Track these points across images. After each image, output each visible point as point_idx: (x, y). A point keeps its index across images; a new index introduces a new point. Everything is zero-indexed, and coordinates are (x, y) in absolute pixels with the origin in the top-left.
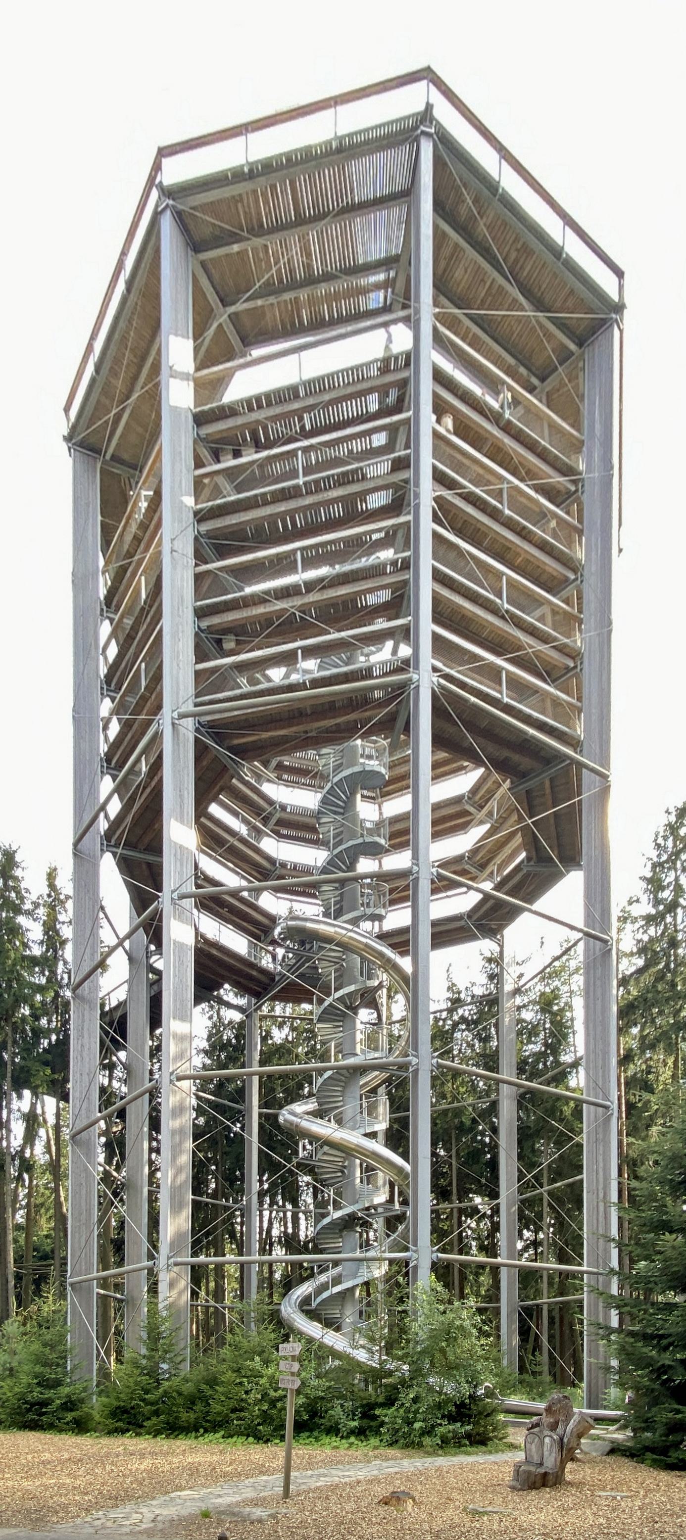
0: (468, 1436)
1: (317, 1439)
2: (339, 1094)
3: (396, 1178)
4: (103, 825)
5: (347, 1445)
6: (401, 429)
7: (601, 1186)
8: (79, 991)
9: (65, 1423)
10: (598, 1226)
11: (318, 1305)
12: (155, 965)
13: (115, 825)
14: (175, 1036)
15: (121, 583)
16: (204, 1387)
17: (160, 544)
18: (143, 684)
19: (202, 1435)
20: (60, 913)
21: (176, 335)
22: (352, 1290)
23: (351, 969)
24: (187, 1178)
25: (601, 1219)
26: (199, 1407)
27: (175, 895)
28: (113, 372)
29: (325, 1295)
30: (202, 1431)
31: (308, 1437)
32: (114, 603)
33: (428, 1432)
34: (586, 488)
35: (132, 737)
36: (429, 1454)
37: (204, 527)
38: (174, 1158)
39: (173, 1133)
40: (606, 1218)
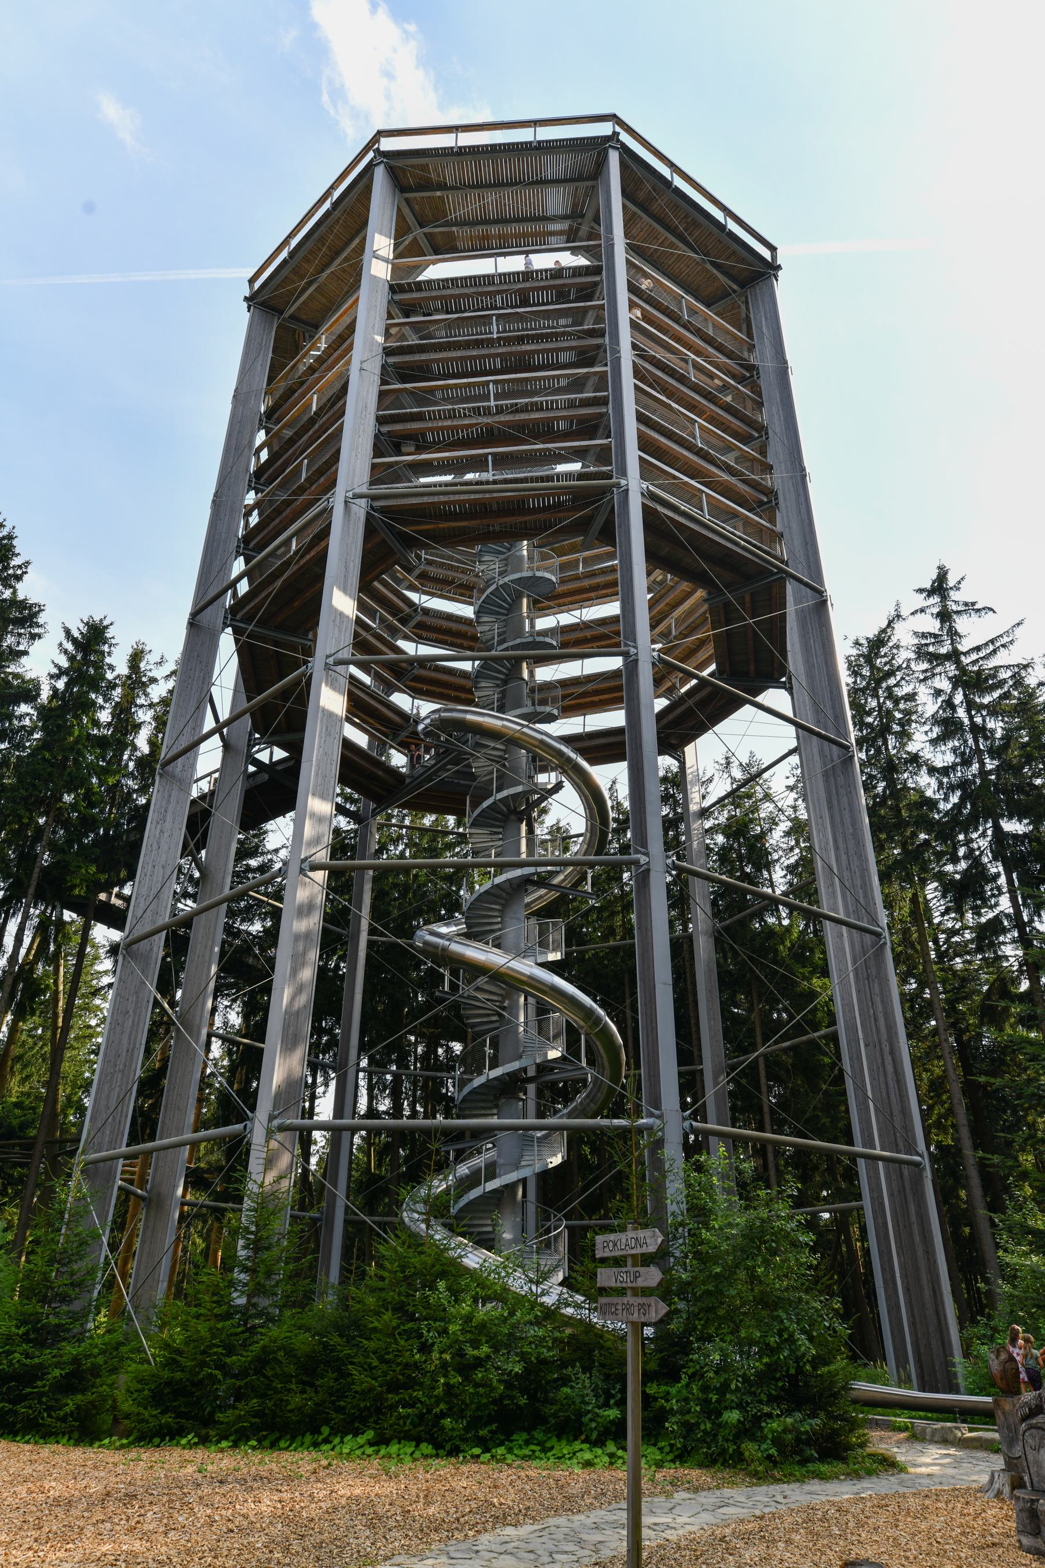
0: (812, 1439)
1: (545, 1450)
2: (496, 914)
3: (582, 1023)
4: (228, 600)
5: (606, 1459)
6: (590, 313)
7: (884, 1037)
8: (169, 768)
9: (58, 1419)
10: (888, 1093)
11: (461, 1210)
12: (257, 756)
13: (240, 603)
14: (313, 815)
15: (286, 401)
16: (335, 1339)
17: (349, 363)
18: (304, 476)
19: (327, 1441)
20: (138, 696)
21: (381, 234)
22: (511, 1187)
23: (515, 769)
24: (308, 1001)
25: (892, 1084)
26: (328, 1380)
27: (331, 660)
28: (306, 260)
29: (475, 1193)
30: (326, 1430)
31: (527, 1443)
32: (276, 416)
33: (749, 1429)
34: (761, 374)
35: (281, 522)
36: (760, 1478)
37: (391, 360)
38: (294, 972)
39: (297, 937)
40: (898, 1081)
